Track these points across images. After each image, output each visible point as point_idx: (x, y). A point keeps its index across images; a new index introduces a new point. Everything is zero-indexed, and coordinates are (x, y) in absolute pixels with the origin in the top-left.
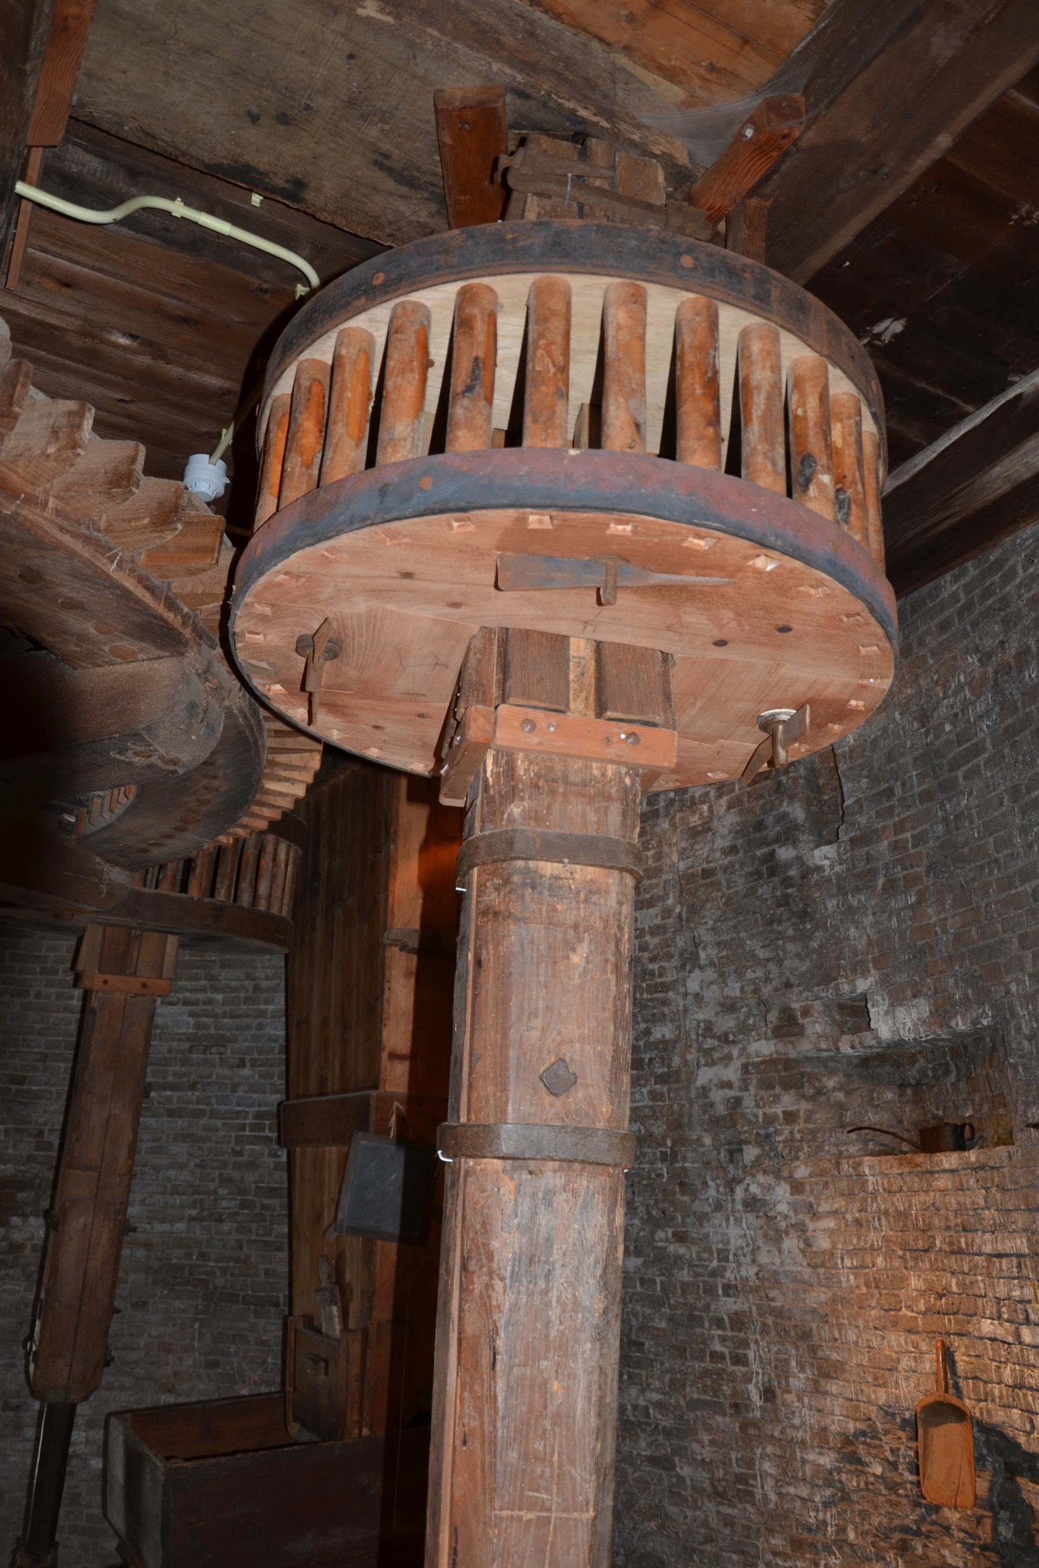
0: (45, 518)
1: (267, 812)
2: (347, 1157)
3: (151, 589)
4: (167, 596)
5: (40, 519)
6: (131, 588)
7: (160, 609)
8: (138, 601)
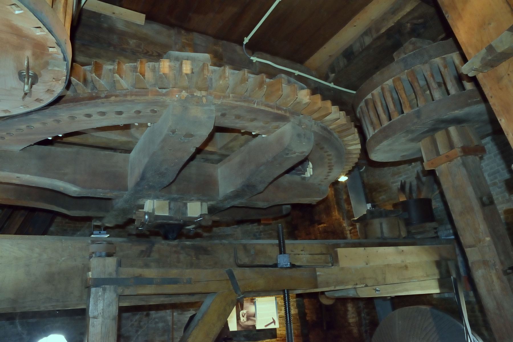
0: (230, 100)
1: (355, 156)
2: (201, 211)
3: (271, 107)
4: (276, 107)
5: (229, 101)
6: (264, 109)
7: (276, 111)
8: (267, 111)
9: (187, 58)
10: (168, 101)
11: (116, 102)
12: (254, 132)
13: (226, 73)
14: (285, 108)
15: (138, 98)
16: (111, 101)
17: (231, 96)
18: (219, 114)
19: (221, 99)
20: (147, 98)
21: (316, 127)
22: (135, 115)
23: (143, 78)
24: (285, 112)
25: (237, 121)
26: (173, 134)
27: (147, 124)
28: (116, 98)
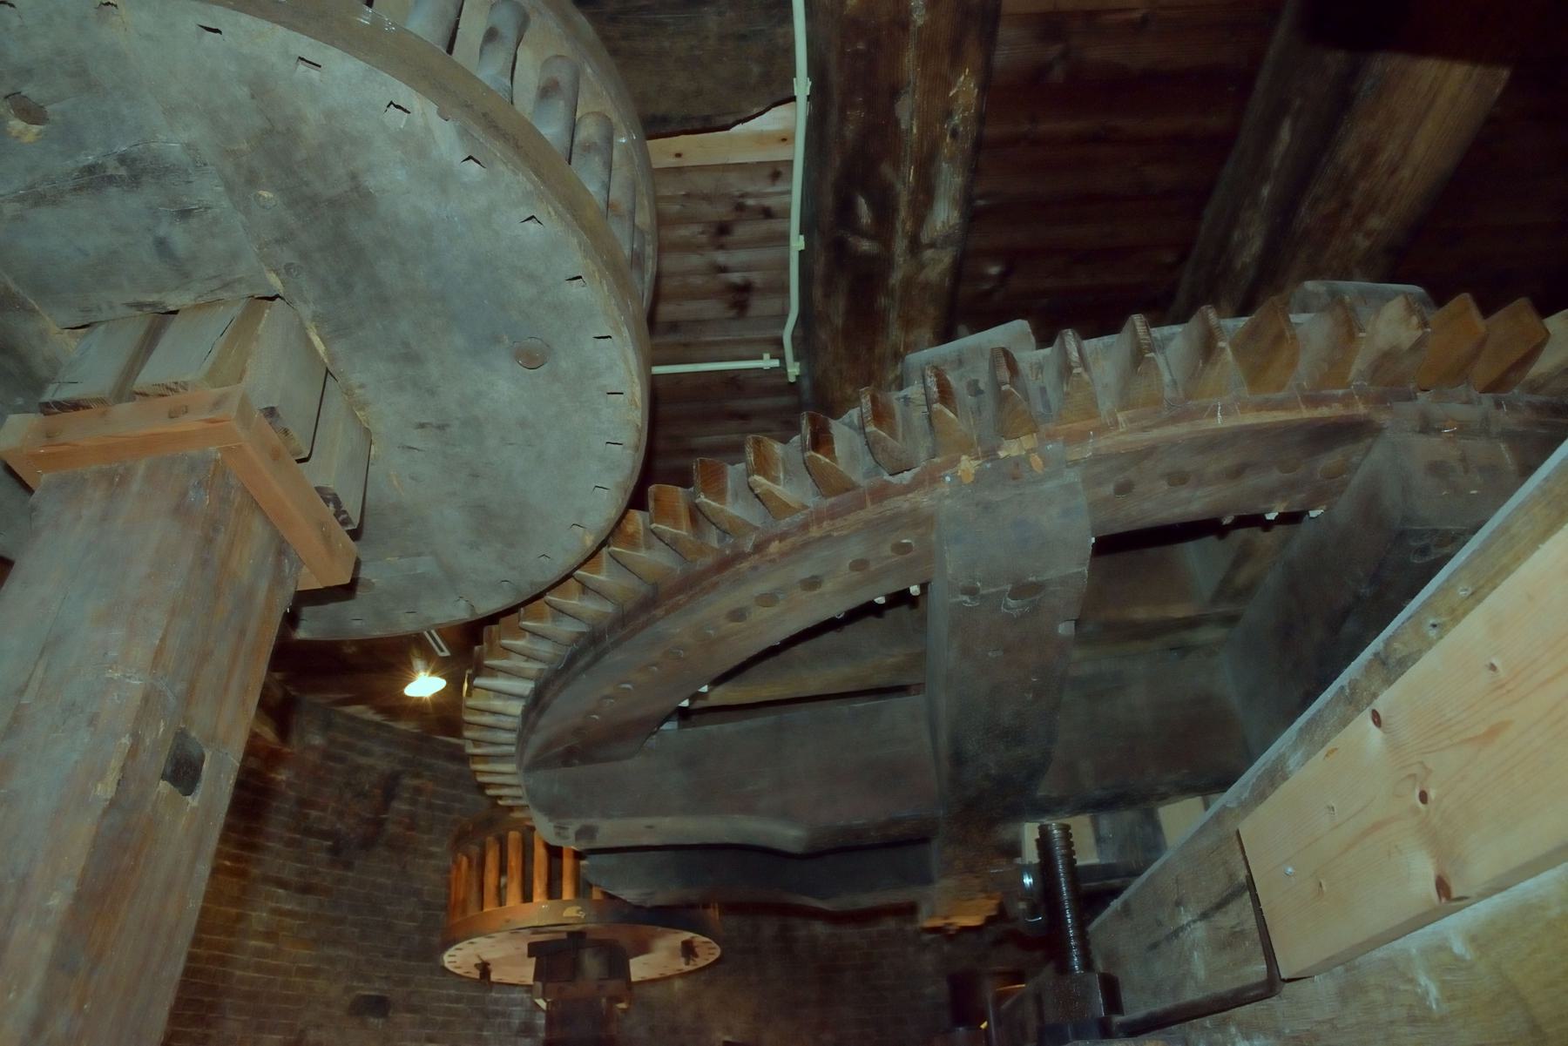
0: (1123, 433)
7: (1306, 414)
9: (958, 355)
10: (925, 503)
11: (783, 554)
12: (1269, 511)
13: (1071, 353)
14: (1340, 392)
15: (839, 522)
16: (772, 557)
17: (1121, 417)
18: (1109, 489)
19: (1091, 441)
20: (862, 514)
21: (1507, 414)
22: (856, 575)
23: (830, 459)
24: (1347, 406)
25: (1184, 493)
26: (973, 599)
27: (908, 589)
28: (783, 543)
